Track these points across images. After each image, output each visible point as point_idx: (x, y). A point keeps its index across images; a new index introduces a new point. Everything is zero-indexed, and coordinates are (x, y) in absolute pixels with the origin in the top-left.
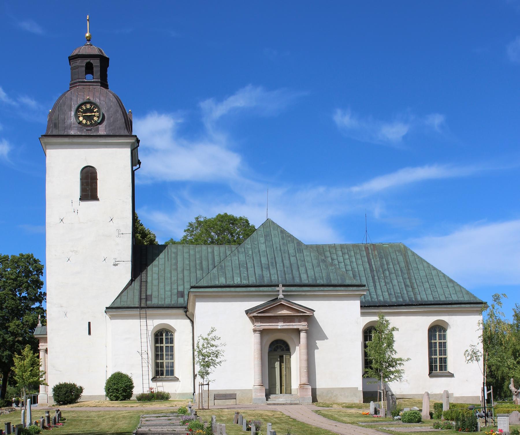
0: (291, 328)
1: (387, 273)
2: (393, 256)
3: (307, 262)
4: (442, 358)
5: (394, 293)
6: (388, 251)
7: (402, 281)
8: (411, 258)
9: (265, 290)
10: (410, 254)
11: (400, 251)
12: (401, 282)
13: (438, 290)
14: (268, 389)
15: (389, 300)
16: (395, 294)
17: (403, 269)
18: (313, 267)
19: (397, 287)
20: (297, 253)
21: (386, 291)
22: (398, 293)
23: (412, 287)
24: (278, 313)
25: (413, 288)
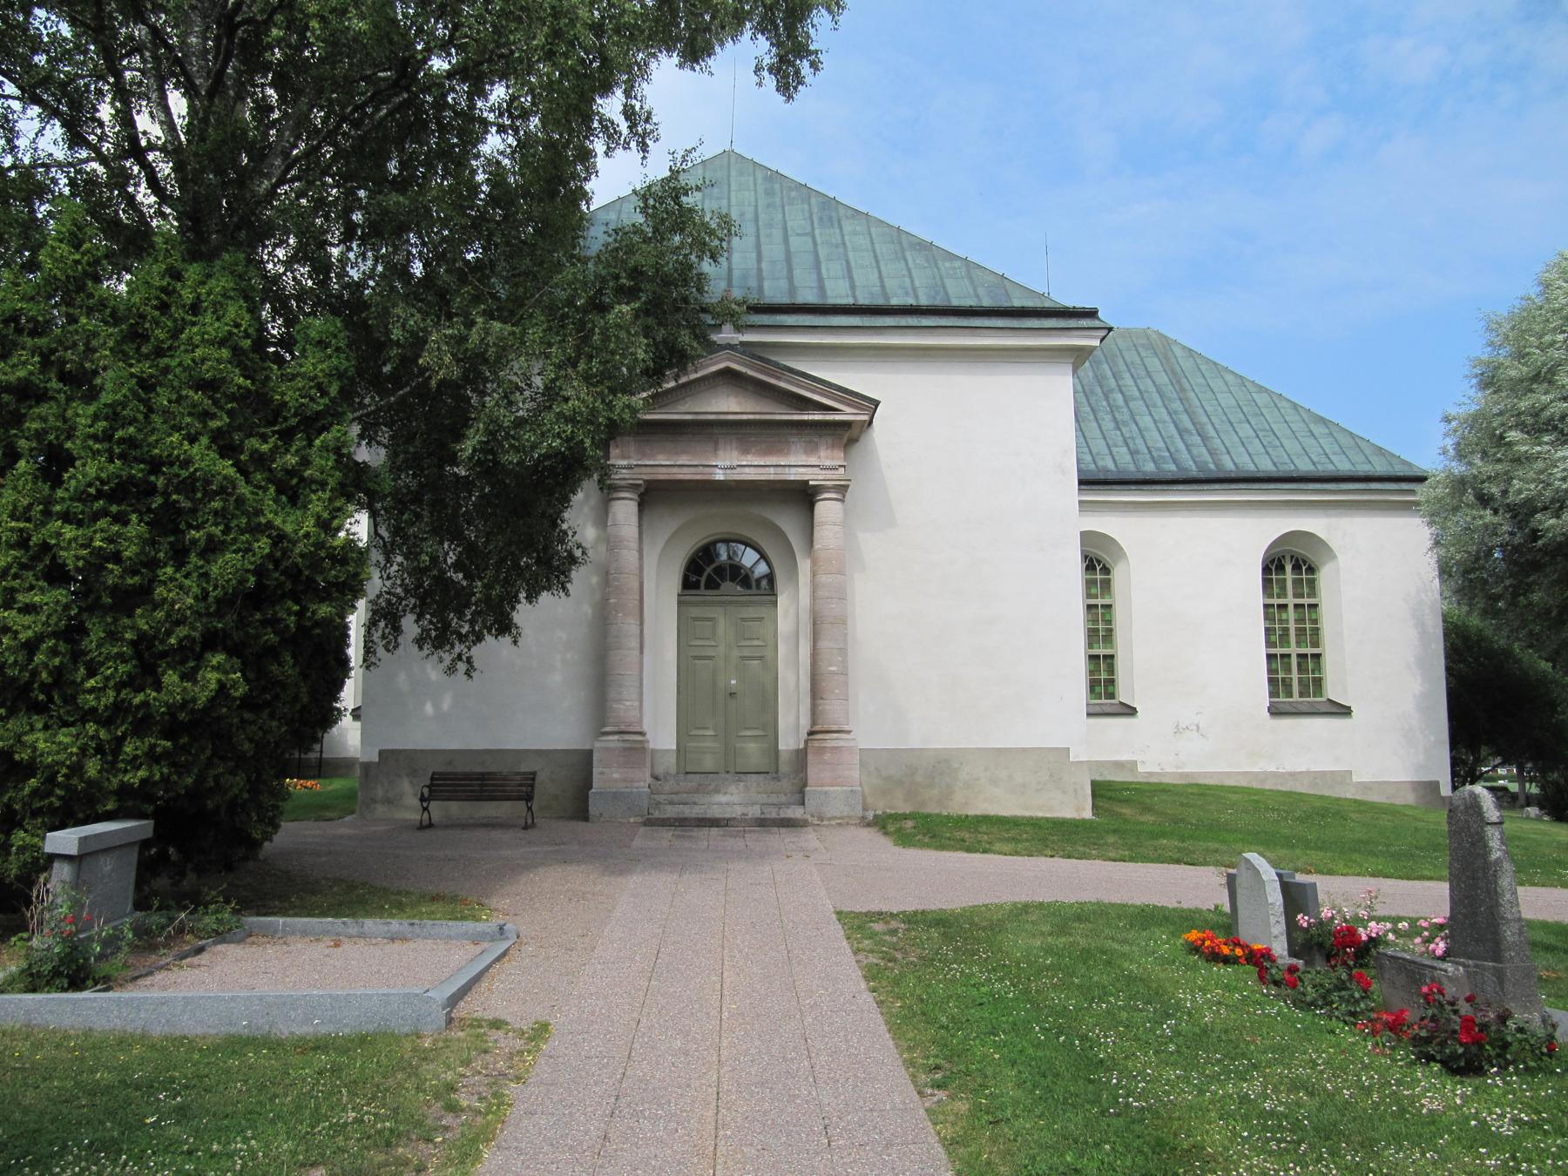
1: (1119, 397)
2: (1131, 356)
3: (854, 249)
4: (1305, 656)
5: (1148, 448)
6: (1114, 347)
7: (1168, 418)
8: (1187, 365)
10: (1178, 352)
11: (1150, 347)
12: (1165, 422)
13: (1286, 443)
14: (667, 751)
15: (1132, 468)
16: (1150, 452)
17: (1164, 388)
18: (877, 262)
19: (1156, 434)
20: (816, 225)
21: (1120, 443)
22: (1159, 449)
23: (1199, 435)
24: (710, 410)
25: (1205, 439)
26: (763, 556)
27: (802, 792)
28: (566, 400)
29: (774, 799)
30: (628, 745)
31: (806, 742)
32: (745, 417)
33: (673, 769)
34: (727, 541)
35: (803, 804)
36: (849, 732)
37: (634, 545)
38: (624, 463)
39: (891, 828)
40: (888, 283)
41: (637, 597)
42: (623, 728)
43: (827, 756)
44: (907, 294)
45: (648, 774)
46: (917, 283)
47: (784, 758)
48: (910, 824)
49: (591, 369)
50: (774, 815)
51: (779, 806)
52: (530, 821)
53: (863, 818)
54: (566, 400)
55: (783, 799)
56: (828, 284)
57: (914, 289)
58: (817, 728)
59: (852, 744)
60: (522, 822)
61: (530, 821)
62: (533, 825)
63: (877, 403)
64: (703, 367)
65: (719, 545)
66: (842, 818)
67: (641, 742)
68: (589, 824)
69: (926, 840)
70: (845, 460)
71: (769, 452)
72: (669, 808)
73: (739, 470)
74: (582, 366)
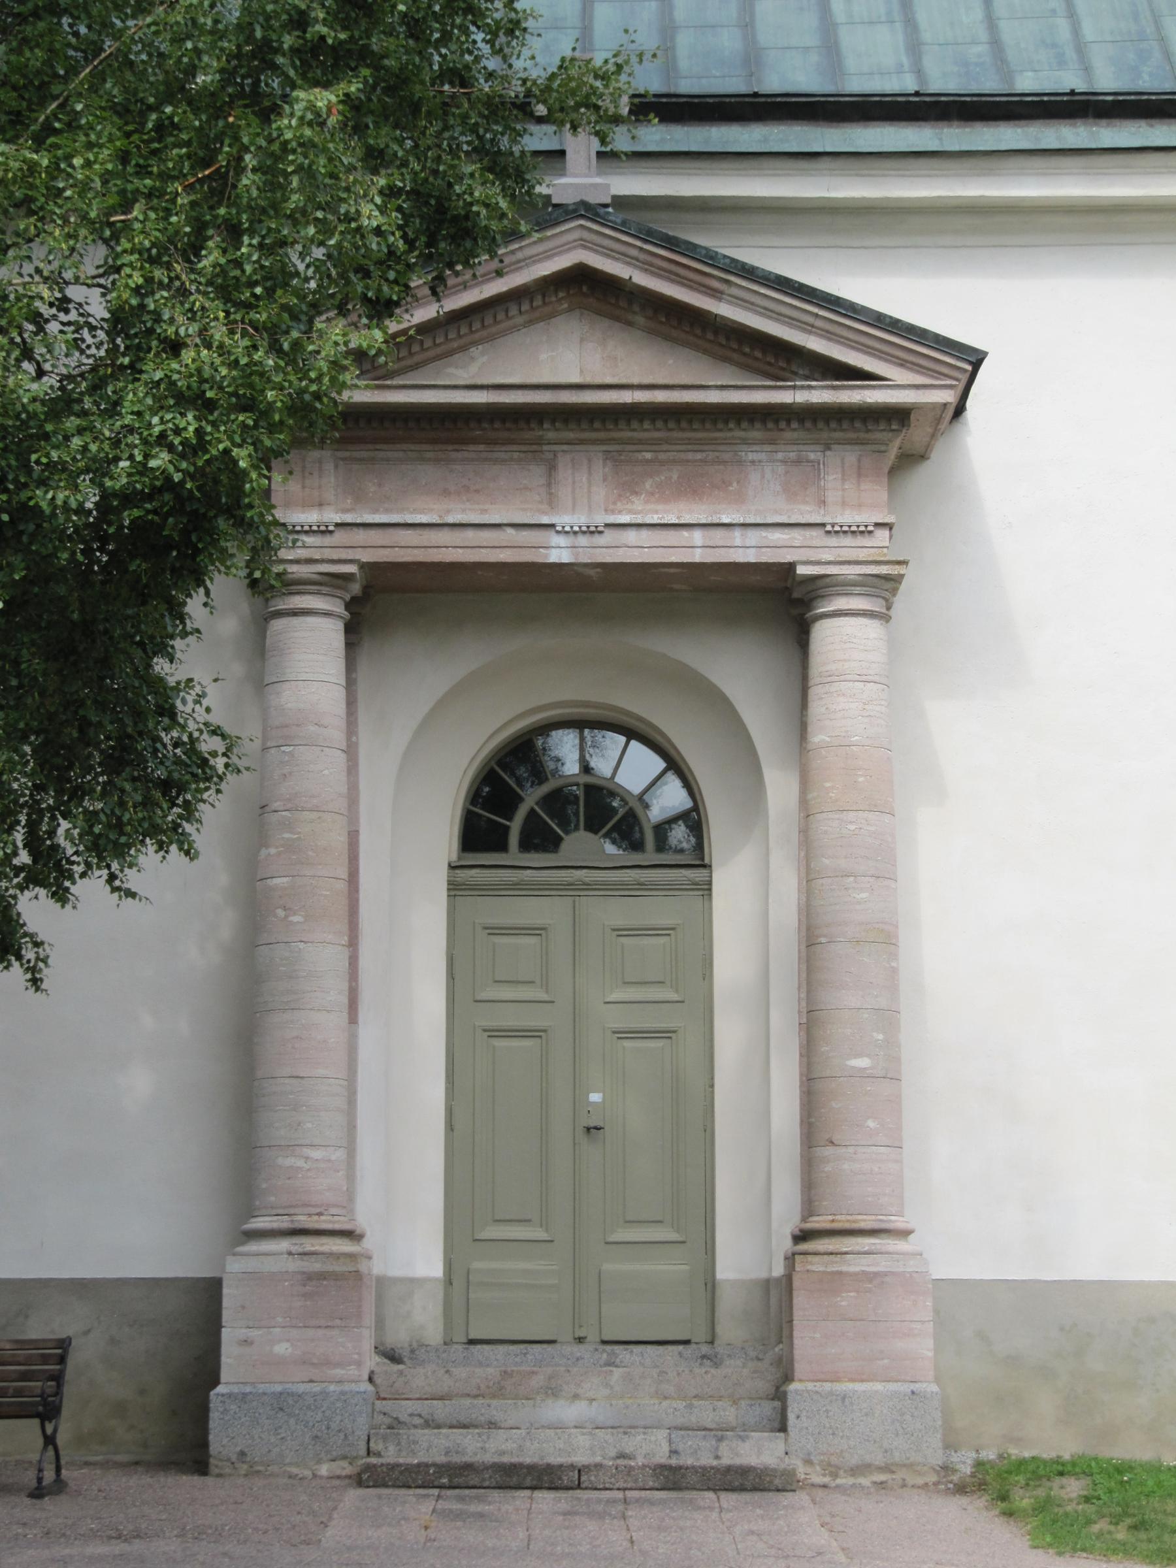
0: (698, 556)
9: (520, 392)
26: (674, 765)
27: (779, 1396)
28: (175, 347)
29: (705, 1414)
30: (316, 1266)
31: (790, 1259)
32: (626, 397)
33: (434, 1333)
34: (579, 724)
35: (783, 1428)
36: (905, 1234)
37: (337, 735)
38: (311, 517)
39: (1023, 1500)
40: (1009, 31)
41: (343, 873)
42: (303, 1221)
43: (846, 1300)
44: (1061, 63)
45: (368, 1344)
46: (1089, 31)
47: (728, 1302)
48: (1073, 1488)
49: (238, 264)
50: (706, 1460)
51: (719, 1432)
52: (49, 1476)
53: (946, 1469)
54: (175, 347)
55: (729, 1414)
56: (850, 40)
57: (1080, 48)
58: (817, 1223)
59: (911, 1266)
60: (29, 1478)
61: (49, 1476)
62: (59, 1486)
63: (976, 359)
64: (518, 266)
65: (556, 735)
66: (887, 1469)
67: (352, 1256)
68: (209, 1480)
69: (1121, 1534)
70: (891, 506)
71: (691, 489)
72: (424, 1436)
73: (609, 537)
74: (211, 258)
